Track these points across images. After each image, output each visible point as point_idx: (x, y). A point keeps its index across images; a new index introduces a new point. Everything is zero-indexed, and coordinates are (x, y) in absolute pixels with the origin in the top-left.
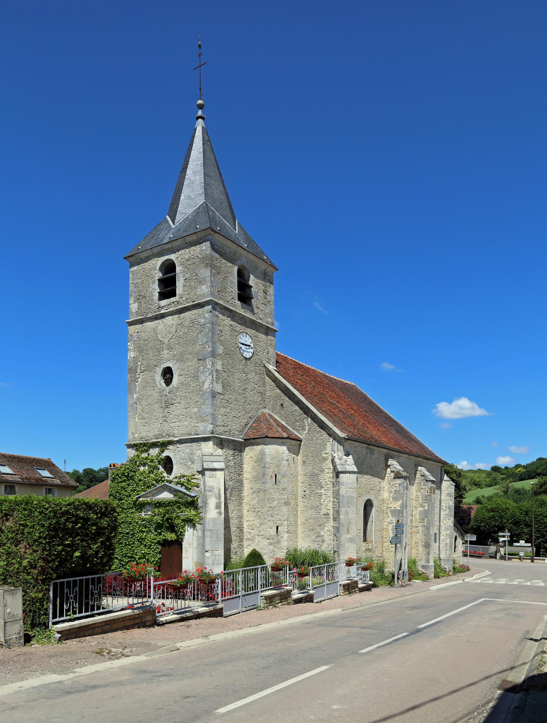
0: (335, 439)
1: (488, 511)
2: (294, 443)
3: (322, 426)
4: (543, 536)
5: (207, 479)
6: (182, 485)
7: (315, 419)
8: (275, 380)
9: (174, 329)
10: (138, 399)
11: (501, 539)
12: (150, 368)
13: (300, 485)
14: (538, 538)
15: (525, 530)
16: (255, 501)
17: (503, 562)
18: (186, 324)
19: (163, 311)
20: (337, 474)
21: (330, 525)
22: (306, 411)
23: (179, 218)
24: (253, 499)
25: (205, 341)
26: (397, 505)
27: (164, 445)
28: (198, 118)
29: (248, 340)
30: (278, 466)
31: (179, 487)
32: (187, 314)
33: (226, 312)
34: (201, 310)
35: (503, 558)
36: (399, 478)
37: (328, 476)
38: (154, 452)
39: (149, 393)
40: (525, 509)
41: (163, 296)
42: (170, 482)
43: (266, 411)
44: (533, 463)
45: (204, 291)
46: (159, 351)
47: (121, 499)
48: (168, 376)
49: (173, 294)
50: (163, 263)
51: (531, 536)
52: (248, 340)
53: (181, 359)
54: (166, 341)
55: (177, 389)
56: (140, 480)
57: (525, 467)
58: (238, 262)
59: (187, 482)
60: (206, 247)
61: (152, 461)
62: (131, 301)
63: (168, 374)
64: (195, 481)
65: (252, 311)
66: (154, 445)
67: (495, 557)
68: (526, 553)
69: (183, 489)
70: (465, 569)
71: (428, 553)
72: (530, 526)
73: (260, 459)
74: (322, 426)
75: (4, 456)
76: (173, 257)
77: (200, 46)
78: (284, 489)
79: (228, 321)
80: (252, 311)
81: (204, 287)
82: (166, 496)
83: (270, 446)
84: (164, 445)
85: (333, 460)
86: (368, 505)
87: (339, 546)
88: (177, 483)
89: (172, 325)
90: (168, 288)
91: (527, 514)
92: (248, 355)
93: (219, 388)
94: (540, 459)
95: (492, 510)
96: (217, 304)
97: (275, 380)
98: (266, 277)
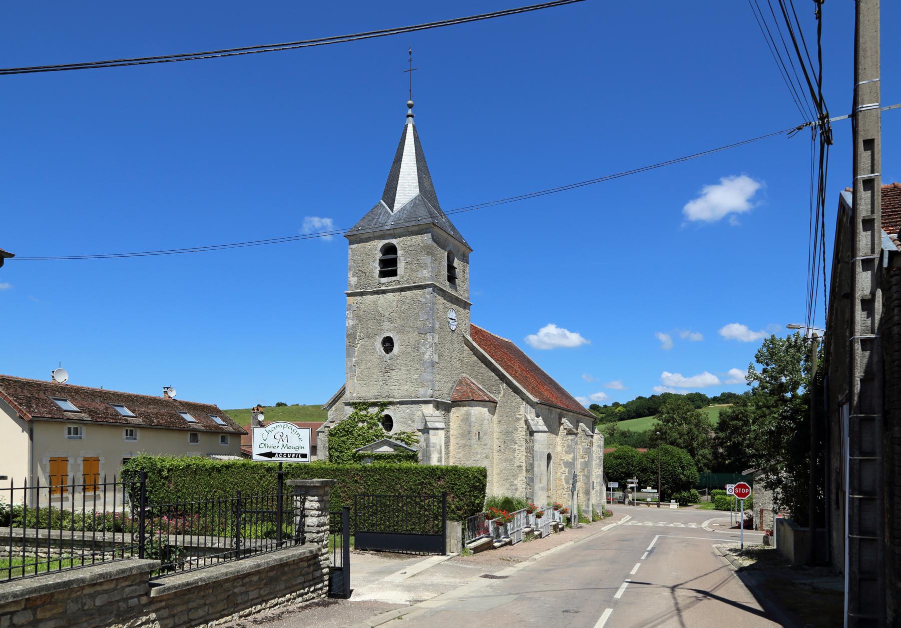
0: (527, 403)
1: (616, 458)
2: (492, 405)
3: (516, 391)
4: (668, 483)
5: (431, 437)
6: (402, 440)
7: (510, 384)
8: (472, 348)
9: (395, 304)
10: (357, 362)
11: (630, 485)
12: (369, 336)
13: (495, 440)
14: (663, 484)
15: (652, 477)
16: (461, 455)
17: (631, 507)
18: (407, 301)
19: (383, 288)
20: (532, 433)
21: (523, 475)
22: (502, 377)
23: (397, 206)
24: (459, 453)
25: (426, 317)
26: (569, 458)
27: (384, 405)
28: (408, 116)
29: (452, 315)
30: (481, 425)
31: (398, 442)
32: (408, 293)
33: (441, 293)
34: (422, 291)
35: (631, 503)
36: (571, 434)
37: (521, 433)
38: (373, 411)
39: (369, 358)
40: (651, 457)
41: (383, 274)
42: (390, 438)
43: (464, 375)
44: (632, 402)
45: (425, 275)
46: (379, 322)
47: (341, 452)
48: (387, 344)
49: (394, 273)
50: (384, 246)
51: (657, 483)
52: (452, 315)
53: (401, 330)
54: (387, 314)
55: (398, 357)
56: (359, 435)
57: (623, 406)
58: (448, 249)
59: (407, 438)
60: (427, 238)
61: (371, 418)
62: (350, 274)
63: (388, 344)
64: (415, 437)
65: (456, 289)
66: (374, 404)
67: (624, 503)
68: (652, 498)
69: (403, 444)
70: (607, 514)
71: (588, 500)
72: (657, 473)
73: (466, 419)
74: (516, 391)
75: (3, 380)
76: (394, 241)
77: (410, 53)
78: (485, 445)
79: (441, 300)
80: (456, 289)
81: (425, 272)
82: (386, 449)
83: (474, 408)
84: (384, 405)
85: (526, 421)
86: (549, 457)
87: (532, 494)
88: (397, 439)
89: (394, 301)
90: (389, 266)
91: (653, 462)
92: (453, 328)
93: (436, 359)
94: (640, 398)
95: (619, 457)
96: (436, 286)
97: (472, 348)
98: (465, 259)
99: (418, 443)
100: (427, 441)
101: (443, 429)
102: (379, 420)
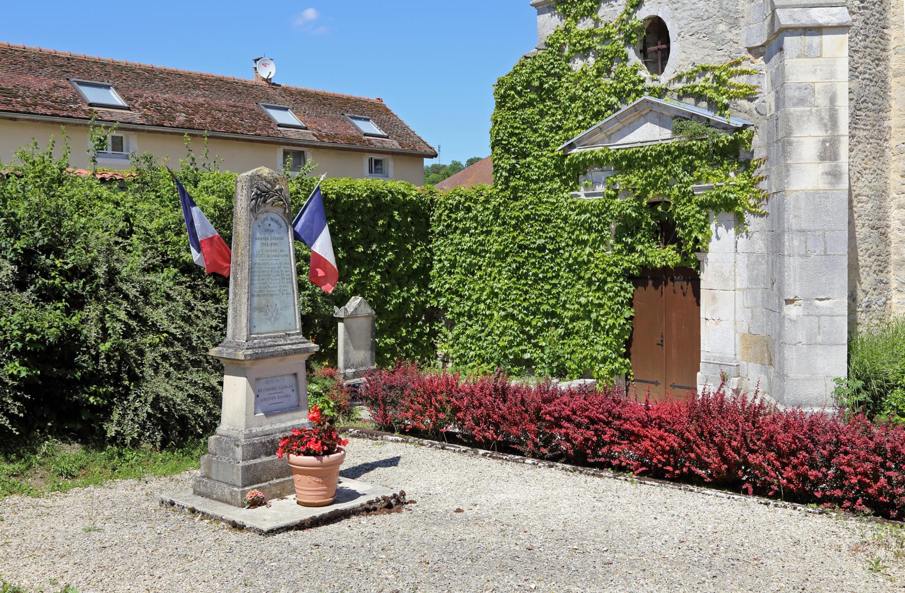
6: (699, 97)
31: (688, 106)
42: (662, 93)
56: (573, 99)
59: (715, 87)
61: (607, 38)
64: (741, 80)
69: (702, 110)
82: (649, 134)
88: (684, 94)
99: (750, 98)
100: (779, 83)
101: (841, 28)
102: (628, 40)
